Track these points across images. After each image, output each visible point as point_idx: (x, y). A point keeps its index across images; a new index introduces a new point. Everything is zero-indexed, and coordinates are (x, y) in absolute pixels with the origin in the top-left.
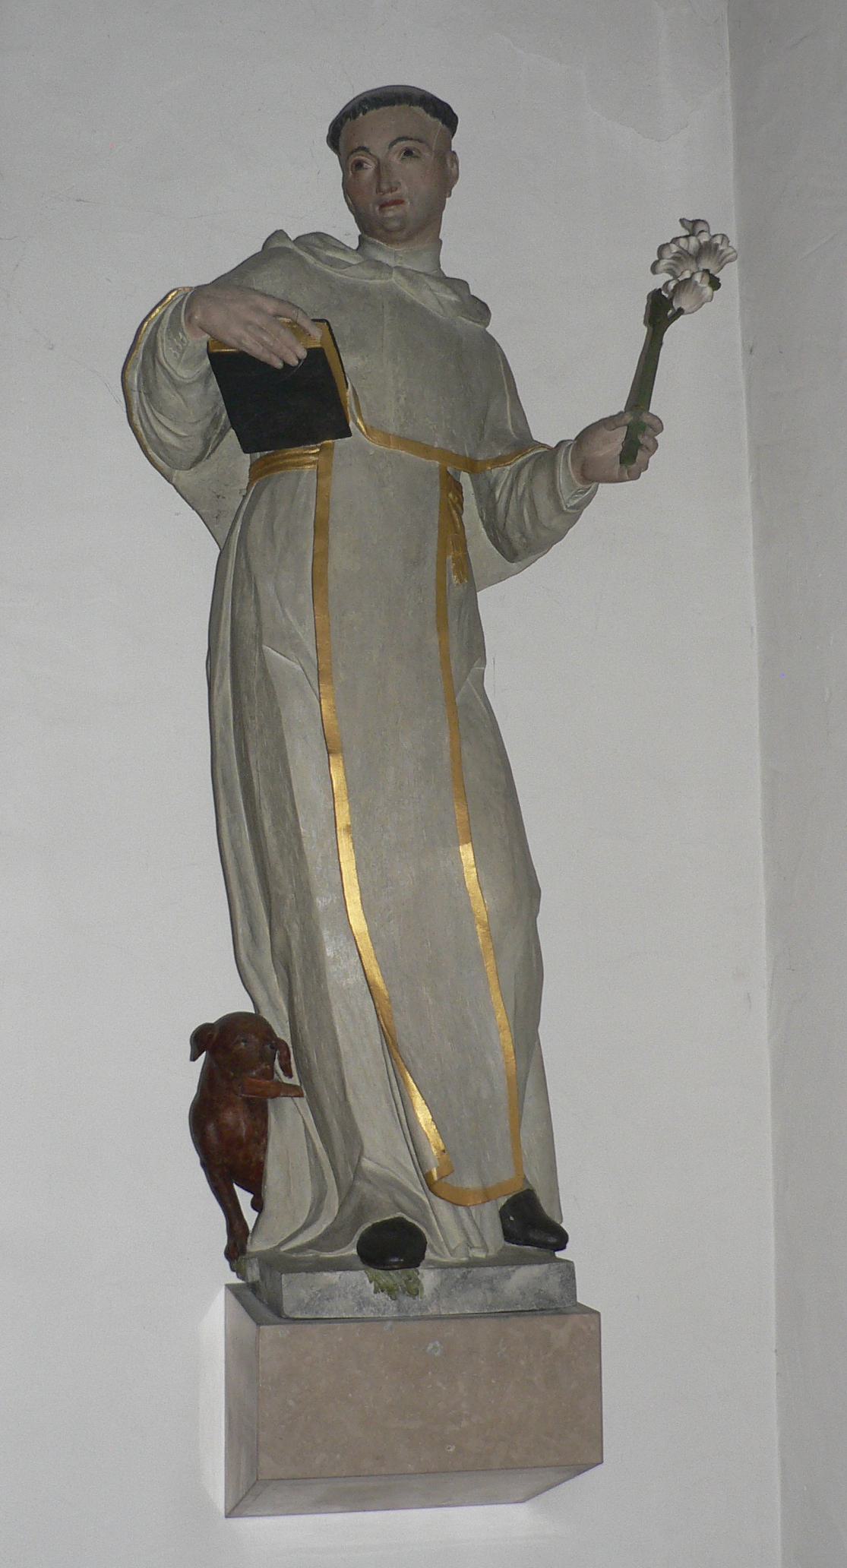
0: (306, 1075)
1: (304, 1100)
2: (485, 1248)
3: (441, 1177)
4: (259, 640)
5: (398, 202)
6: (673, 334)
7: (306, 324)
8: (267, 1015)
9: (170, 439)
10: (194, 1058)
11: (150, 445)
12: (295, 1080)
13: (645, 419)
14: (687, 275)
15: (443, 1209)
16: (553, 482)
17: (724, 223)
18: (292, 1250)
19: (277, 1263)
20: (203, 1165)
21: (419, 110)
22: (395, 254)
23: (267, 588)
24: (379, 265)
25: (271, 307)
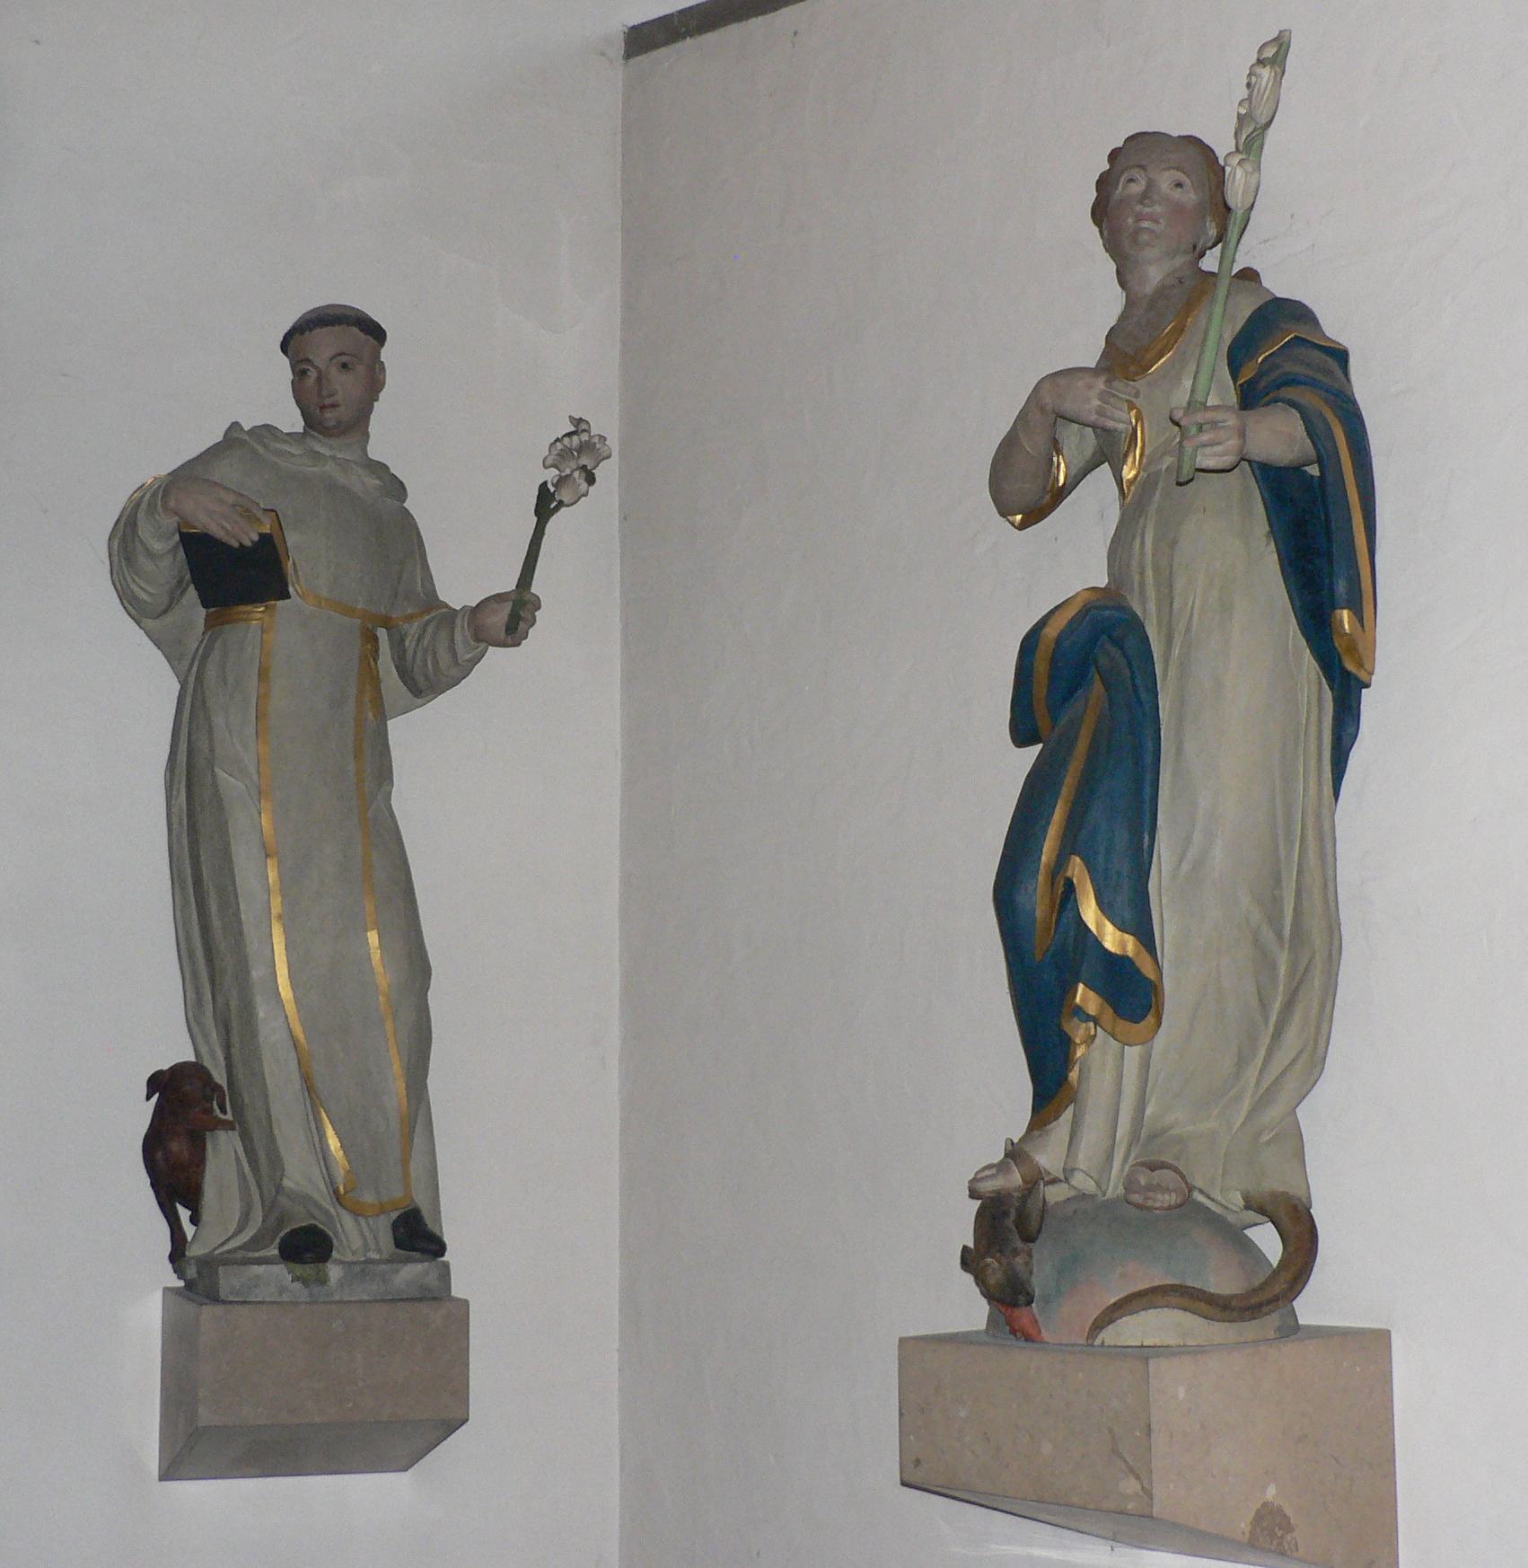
0: (238, 1110)
1: (236, 1133)
2: (379, 1251)
3: (346, 1192)
4: (211, 764)
5: (334, 406)
6: (552, 525)
7: (259, 514)
8: (207, 1063)
9: (144, 596)
10: (148, 1098)
11: (128, 599)
12: (229, 1117)
13: (527, 597)
14: (568, 471)
15: (347, 1220)
16: (452, 640)
17: (607, 424)
18: (229, 1252)
19: (209, 1264)
20: (152, 1185)
21: (355, 330)
22: (331, 447)
23: (218, 721)
24: (316, 455)
25: (231, 499)
